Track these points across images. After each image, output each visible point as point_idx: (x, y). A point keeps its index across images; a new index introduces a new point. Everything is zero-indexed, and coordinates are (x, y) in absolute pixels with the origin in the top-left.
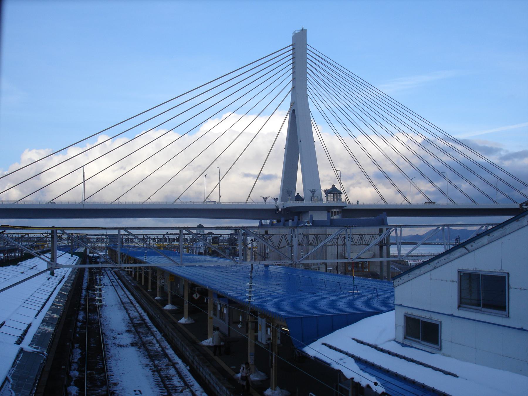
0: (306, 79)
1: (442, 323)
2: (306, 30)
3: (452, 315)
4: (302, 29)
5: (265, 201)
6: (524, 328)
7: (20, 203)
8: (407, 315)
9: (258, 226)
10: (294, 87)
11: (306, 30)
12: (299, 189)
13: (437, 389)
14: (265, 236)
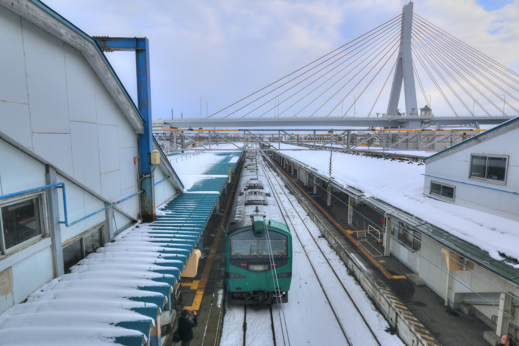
0: (411, 37)
1: (456, 187)
2: (413, 2)
3: (464, 183)
4: (410, 2)
5: (378, 116)
6: (517, 193)
7: (225, 119)
8: (433, 182)
9: (316, 131)
10: (402, 43)
11: (413, 2)
12: (402, 107)
13: (68, 174)
14: (464, 136)
